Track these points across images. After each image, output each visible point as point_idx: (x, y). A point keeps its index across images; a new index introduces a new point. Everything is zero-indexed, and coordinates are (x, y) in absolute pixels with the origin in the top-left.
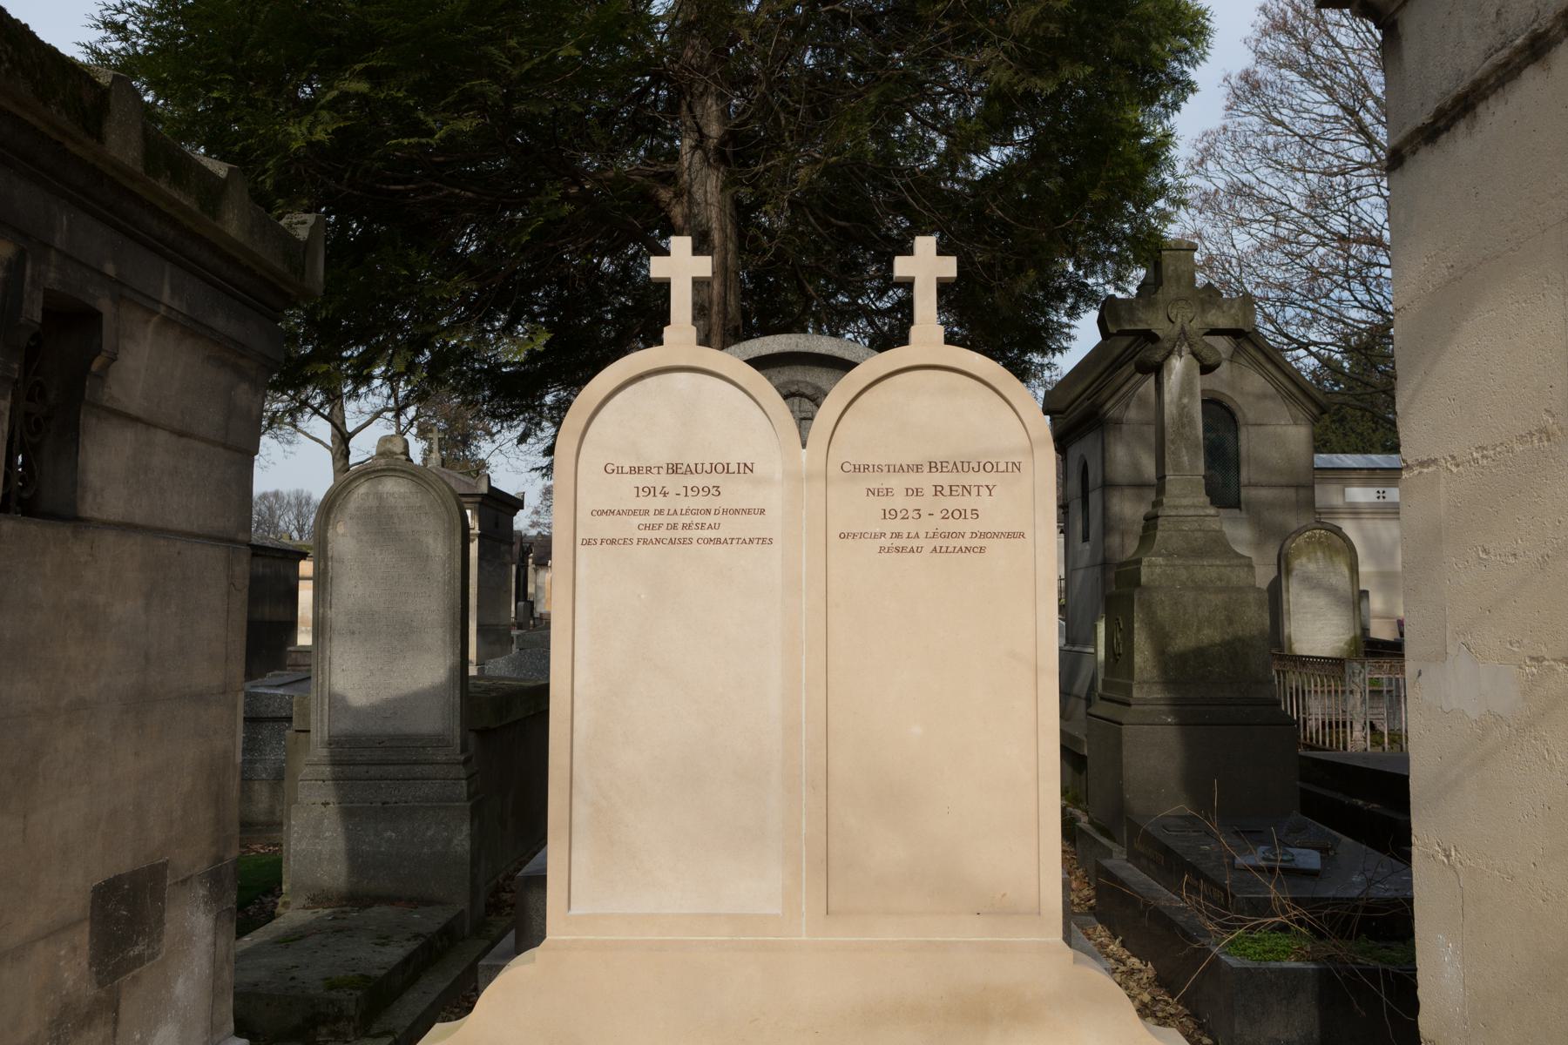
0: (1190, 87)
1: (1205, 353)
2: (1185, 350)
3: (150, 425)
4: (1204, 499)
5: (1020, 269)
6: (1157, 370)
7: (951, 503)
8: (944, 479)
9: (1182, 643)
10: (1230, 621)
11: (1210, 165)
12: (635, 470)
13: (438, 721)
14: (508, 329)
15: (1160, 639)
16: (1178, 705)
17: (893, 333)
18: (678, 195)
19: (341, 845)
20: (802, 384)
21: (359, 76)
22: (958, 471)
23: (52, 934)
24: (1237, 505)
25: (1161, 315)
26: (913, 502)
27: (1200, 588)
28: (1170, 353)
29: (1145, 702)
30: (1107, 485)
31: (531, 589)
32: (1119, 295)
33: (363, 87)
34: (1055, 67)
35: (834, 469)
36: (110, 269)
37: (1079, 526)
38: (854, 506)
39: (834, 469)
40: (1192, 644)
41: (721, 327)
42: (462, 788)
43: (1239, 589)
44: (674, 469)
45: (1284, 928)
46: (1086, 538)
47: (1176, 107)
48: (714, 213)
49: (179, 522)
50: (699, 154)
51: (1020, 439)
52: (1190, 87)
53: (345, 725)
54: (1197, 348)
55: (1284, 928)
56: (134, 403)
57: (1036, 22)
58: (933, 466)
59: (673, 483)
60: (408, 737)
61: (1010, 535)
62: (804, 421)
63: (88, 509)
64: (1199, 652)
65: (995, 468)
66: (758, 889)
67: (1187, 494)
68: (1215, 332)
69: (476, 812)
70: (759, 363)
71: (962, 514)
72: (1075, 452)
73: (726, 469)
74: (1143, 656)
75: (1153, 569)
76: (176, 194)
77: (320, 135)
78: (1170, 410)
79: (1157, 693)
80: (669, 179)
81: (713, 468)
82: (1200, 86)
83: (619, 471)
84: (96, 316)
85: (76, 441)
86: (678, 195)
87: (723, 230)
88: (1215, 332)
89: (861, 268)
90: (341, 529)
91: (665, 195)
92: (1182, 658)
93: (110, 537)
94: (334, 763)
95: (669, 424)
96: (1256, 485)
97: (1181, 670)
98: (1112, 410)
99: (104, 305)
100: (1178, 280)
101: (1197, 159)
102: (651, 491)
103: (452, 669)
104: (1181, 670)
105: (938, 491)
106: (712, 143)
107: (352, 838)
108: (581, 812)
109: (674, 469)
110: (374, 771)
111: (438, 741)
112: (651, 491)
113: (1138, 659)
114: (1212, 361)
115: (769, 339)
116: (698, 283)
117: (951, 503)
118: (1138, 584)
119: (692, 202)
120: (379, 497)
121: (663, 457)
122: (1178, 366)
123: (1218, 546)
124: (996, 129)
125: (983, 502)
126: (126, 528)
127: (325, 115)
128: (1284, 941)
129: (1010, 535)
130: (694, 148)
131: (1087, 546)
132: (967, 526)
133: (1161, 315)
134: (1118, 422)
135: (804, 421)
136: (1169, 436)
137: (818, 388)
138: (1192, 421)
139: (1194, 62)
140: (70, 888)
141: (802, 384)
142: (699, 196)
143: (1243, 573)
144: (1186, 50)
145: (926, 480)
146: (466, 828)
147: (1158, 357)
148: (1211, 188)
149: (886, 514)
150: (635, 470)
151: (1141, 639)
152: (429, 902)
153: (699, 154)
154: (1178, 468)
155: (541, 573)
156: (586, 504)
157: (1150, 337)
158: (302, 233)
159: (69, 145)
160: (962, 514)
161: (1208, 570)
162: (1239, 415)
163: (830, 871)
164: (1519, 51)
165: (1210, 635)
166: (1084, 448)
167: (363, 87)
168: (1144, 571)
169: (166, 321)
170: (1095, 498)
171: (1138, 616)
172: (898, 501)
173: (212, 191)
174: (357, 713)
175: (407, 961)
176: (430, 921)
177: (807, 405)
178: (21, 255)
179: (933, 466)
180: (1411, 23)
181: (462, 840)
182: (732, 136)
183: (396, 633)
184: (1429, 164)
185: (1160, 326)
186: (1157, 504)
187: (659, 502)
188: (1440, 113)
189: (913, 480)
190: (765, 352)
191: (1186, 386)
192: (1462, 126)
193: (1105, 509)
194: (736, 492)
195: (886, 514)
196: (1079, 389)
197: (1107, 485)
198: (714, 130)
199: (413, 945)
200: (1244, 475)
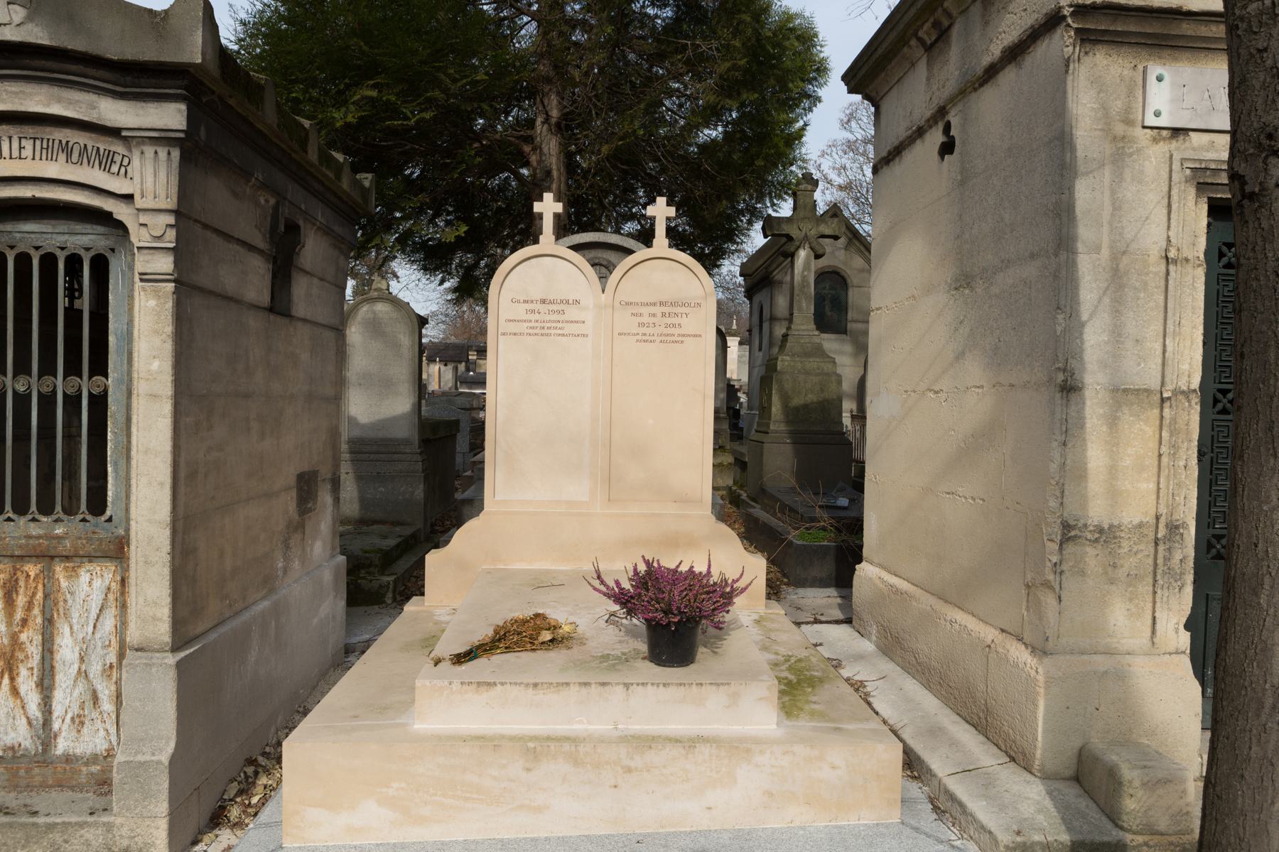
0: (819, 99)
1: (817, 248)
2: (807, 246)
3: (312, 275)
4: (813, 326)
5: (719, 199)
6: (792, 255)
7: (669, 321)
8: (666, 309)
9: (796, 401)
10: (822, 390)
11: (853, 124)
12: (525, 302)
13: (406, 432)
14: (432, 221)
15: (785, 398)
16: (792, 434)
17: (646, 237)
18: (534, 149)
19: (356, 494)
20: (603, 260)
21: (374, 87)
22: (672, 306)
23: (287, 489)
24: (845, 332)
25: (795, 226)
26: (652, 320)
27: (807, 373)
28: (798, 248)
29: (776, 432)
30: (773, 319)
31: (424, 376)
32: (774, 214)
33: (374, 93)
34: (739, 94)
35: (617, 304)
36: (303, 207)
37: (757, 343)
38: (625, 321)
39: (617, 304)
40: (802, 402)
41: (563, 228)
42: (419, 466)
43: (828, 374)
44: (543, 302)
45: (824, 529)
46: (760, 350)
47: (810, 110)
48: (554, 160)
49: (320, 320)
50: (546, 126)
51: (700, 292)
52: (819, 99)
53: (356, 433)
54: (814, 245)
55: (824, 529)
56: (308, 267)
57: (729, 70)
58: (661, 304)
59: (543, 308)
60: (391, 440)
61: (695, 336)
62: (603, 278)
63: (294, 313)
64: (805, 406)
65: (689, 305)
66: (578, 490)
67: (804, 323)
68: (823, 236)
69: (426, 478)
70: (576, 248)
71: (674, 326)
72: (757, 298)
73: (567, 302)
74: (776, 408)
75: (784, 362)
76: (328, 173)
77: (350, 119)
78: (797, 278)
79: (783, 427)
80: (529, 139)
81: (562, 302)
82: (823, 99)
83: (518, 302)
84: (299, 227)
85: (290, 282)
86: (534, 149)
87: (559, 170)
88: (823, 236)
89: (634, 191)
90: (353, 329)
91: (527, 149)
92: (797, 409)
93: (300, 324)
94: (351, 453)
95: (540, 279)
96: (856, 321)
97: (795, 415)
98: (777, 275)
99: (301, 223)
100: (805, 207)
101: (845, 120)
102: (533, 311)
103: (413, 405)
104: (795, 415)
105: (663, 315)
106: (554, 121)
107: (362, 493)
108: (500, 454)
109: (543, 302)
110: (372, 456)
111: (406, 442)
112: (533, 311)
113: (774, 409)
114: (820, 252)
115: (584, 235)
116: (557, 216)
117: (669, 321)
118: (776, 370)
119: (541, 153)
120: (374, 313)
121: (538, 296)
122: (802, 254)
123: (819, 352)
124: (711, 115)
125: (684, 321)
126: (305, 321)
127: (352, 108)
128: (822, 534)
129: (695, 336)
130: (543, 123)
131: (761, 354)
132: (676, 331)
133: (795, 226)
134: (781, 283)
135: (603, 278)
136: (796, 292)
137: (609, 262)
138: (808, 285)
139: (820, 86)
140: (287, 475)
141: (603, 260)
142: (545, 150)
143: (830, 366)
144: (815, 79)
145: (658, 310)
146: (421, 486)
147: (792, 250)
148: (852, 138)
149: (641, 325)
150: (525, 302)
151: (775, 399)
152: (402, 524)
153: (546, 126)
154: (800, 309)
155: (432, 366)
156: (504, 316)
157: (789, 238)
158: (367, 184)
159: (294, 155)
160: (674, 326)
161: (812, 363)
162: (849, 281)
163: (610, 483)
164: (914, 132)
165: (811, 398)
166: (760, 297)
167: (374, 93)
168: (779, 363)
169: (319, 228)
170: (766, 326)
171: (775, 387)
172: (645, 319)
173: (338, 168)
174: (363, 426)
175: (398, 546)
176: (408, 531)
177: (604, 270)
178: (278, 203)
179: (661, 304)
180: (885, 106)
181: (419, 492)
182: (566, 116)
183: (386, 385)
184: (885, 171)
185: (794, 233)
186: (789, 328)
187: (537, 317)
188: (890, 153)
189: (652, 310)
190: (582, 241)
191: (807, 266)
192: (897, 159)
193: (771, 333)
194: (572, 313)
195: (641, 325)
196: (761, 262)
197: (773, 319)
198: (555, 113)
199: (399, 540)
200: (850, 316)
